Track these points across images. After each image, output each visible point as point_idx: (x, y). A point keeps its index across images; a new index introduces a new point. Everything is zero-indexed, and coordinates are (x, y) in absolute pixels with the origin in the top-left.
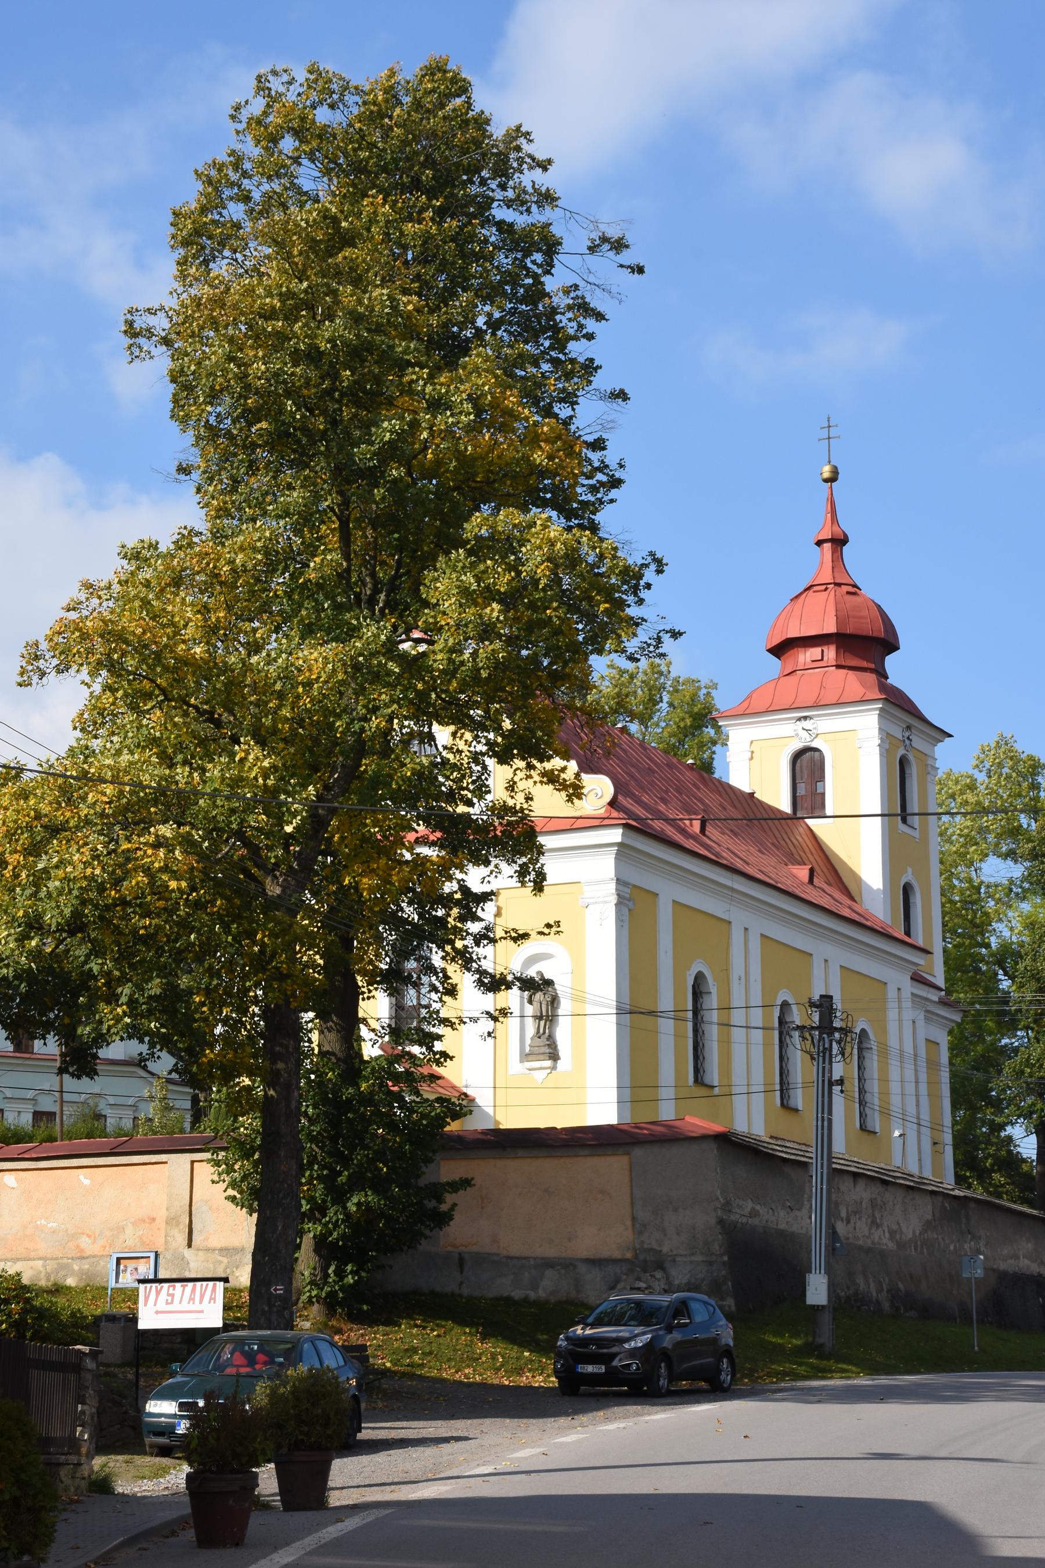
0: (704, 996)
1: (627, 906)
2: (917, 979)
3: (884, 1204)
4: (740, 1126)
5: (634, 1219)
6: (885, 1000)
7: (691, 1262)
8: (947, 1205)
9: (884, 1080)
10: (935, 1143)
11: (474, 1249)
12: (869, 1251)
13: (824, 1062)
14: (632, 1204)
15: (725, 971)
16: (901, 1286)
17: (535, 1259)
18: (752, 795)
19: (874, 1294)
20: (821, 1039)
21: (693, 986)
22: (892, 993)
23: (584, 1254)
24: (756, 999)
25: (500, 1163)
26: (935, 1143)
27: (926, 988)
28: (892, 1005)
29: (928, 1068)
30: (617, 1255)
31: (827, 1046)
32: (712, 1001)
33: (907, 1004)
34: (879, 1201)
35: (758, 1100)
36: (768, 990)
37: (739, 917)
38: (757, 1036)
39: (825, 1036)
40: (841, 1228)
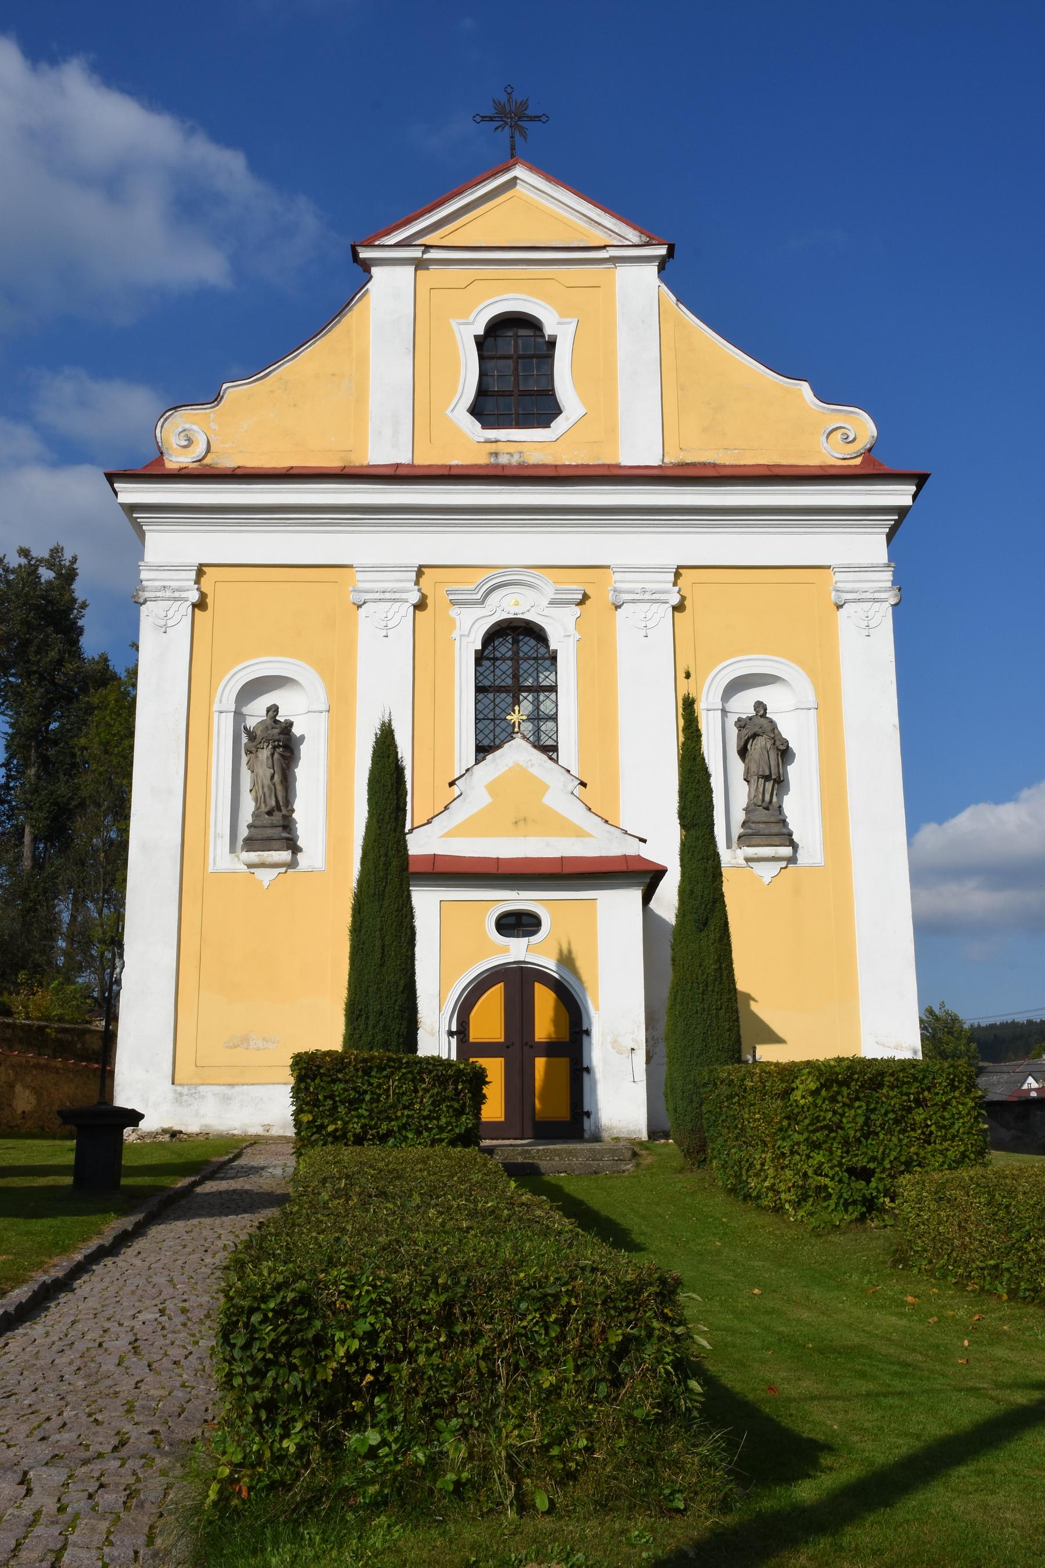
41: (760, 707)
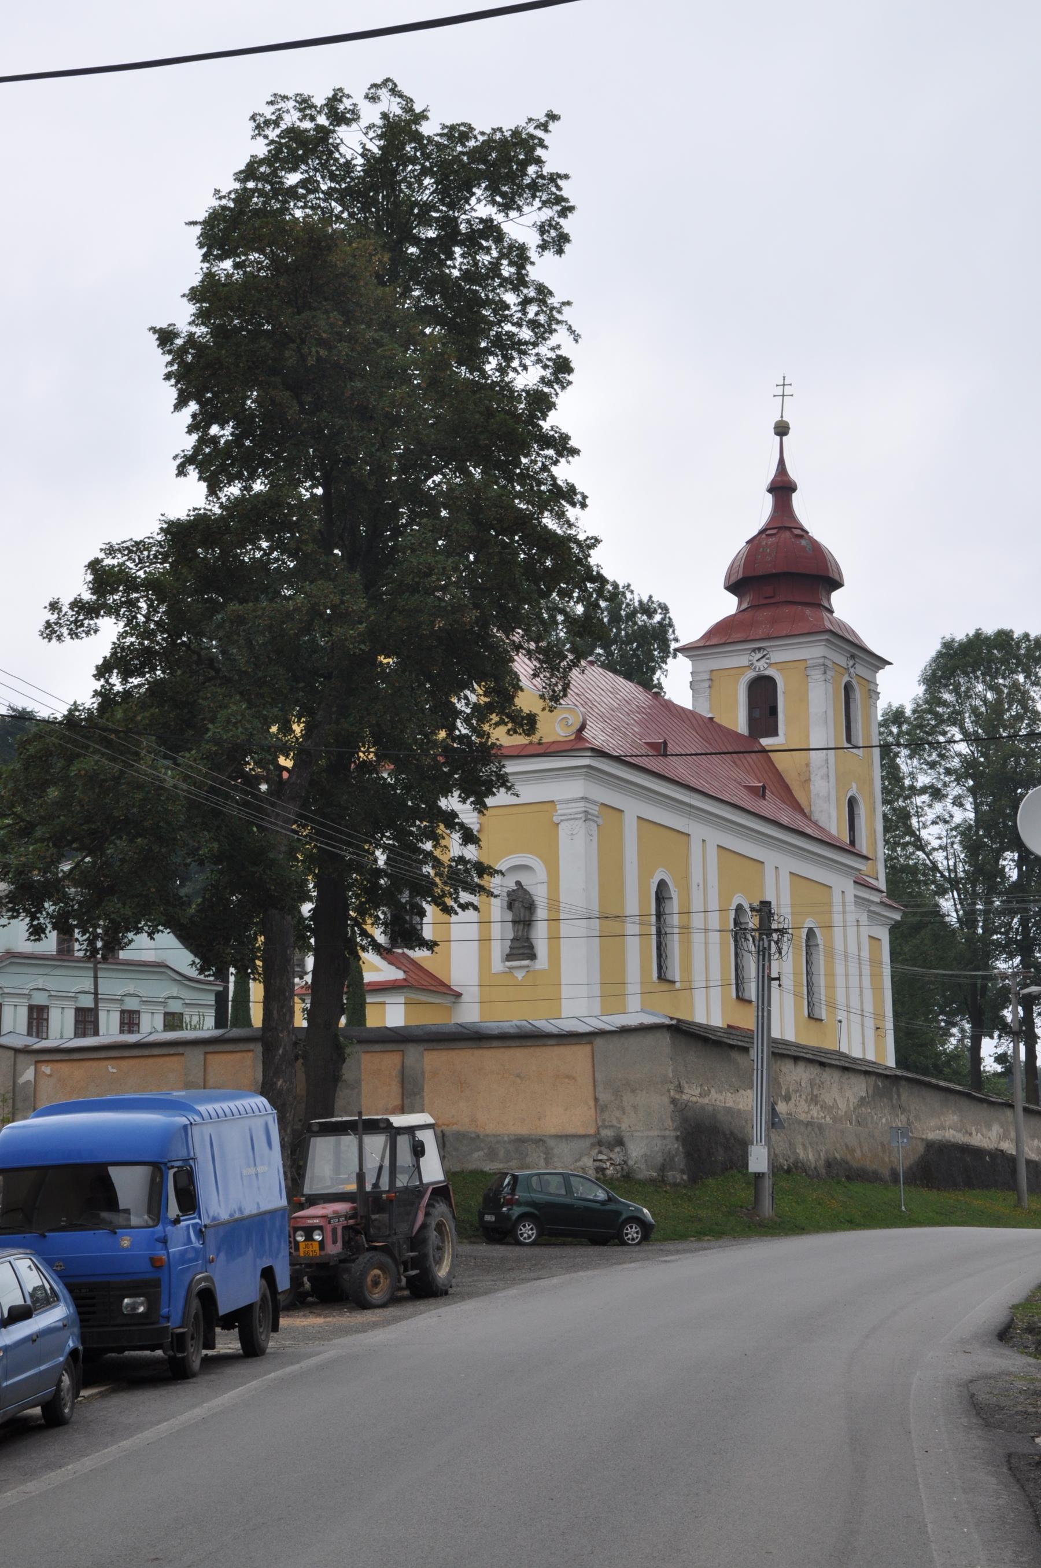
0: (666, 901)
1: (596, 822)
2: (859, 883)
3: (822, 1083)
4: (700, 1018)
5: (596, 1100)
6: (830, 904)
7: (648, 1137)
8: (880, 1084)
9: (831, 974)
10: (878, 1028)
11: (455, 1127)
12: (808, 1124)
13: (764, 960)
14: (595, 1086)
15: (685, 878)
16: (838, 1156)
17: (509, 1136)
18: (711, 719)
19: (813, 1161)
20: (761, 939)
21: (657, 893)
22: (837, 898)
23: (553, 1131)
24: (714, 904)
25: (478, 1053)
26: (878, 1028)
27: (869, 891)
28: (837, 908)
29: (870, 966)
30: (581, 1131)
31: (766, 945)
32: (674, 905)
33: (851, 907)
34: (817, 1081)
35: (716, 994)
36: (724, 895)
37: (697, 830)
38: (715, 937)
39: (764, 937)
40: (782, 1107)
41: (518, 883)
